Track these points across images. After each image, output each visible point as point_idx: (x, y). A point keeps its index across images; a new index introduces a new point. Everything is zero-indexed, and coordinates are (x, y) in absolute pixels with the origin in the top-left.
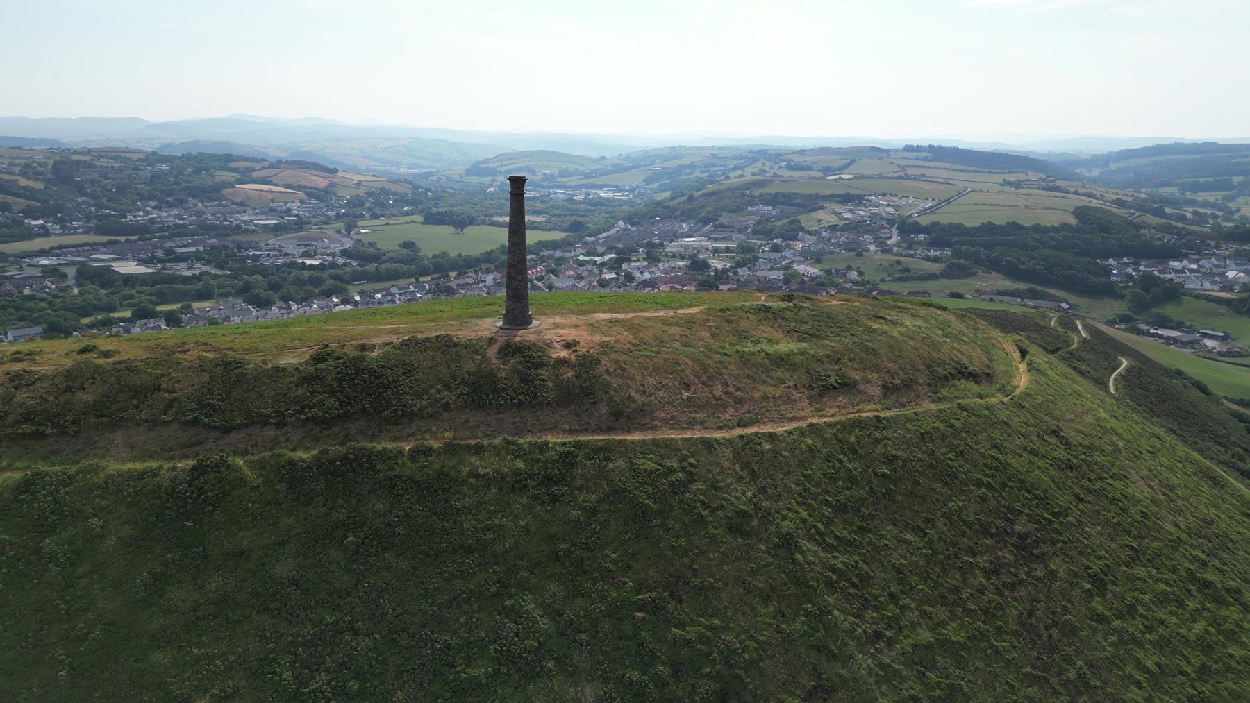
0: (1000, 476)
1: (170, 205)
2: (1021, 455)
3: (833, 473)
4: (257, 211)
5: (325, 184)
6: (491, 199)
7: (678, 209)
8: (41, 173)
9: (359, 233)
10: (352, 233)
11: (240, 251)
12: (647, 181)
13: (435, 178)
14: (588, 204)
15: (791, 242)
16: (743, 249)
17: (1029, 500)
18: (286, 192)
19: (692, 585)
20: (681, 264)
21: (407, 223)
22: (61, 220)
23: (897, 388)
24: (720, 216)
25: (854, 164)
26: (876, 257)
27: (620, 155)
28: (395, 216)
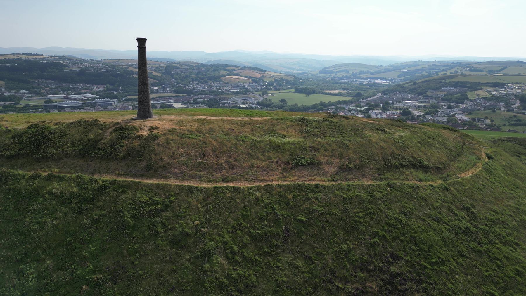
0: (396, 232)
1: (202, 83)
2: (424, 220)
3: (264, 216)
4: (232, 86)
5: (260, 76)
6: (326, 83)
7: (408, 88)
8: (161, 70)
9: (267, 96)
10: (265, 95)
11: (220, 101)
12: (399, 76)
13: (306, 75)
14: (368, 86)
15: (459, 105)
16: (432, 107)
17: (414, 251)
19: (127, 274)
20: (399, 112)
21: (288, 92)
22: (164, 87)
23: (350, 169)
24: (427, 91)
25: (506, 69)
26: (503, 113)
27: (390, 65)
28: (284, 89)
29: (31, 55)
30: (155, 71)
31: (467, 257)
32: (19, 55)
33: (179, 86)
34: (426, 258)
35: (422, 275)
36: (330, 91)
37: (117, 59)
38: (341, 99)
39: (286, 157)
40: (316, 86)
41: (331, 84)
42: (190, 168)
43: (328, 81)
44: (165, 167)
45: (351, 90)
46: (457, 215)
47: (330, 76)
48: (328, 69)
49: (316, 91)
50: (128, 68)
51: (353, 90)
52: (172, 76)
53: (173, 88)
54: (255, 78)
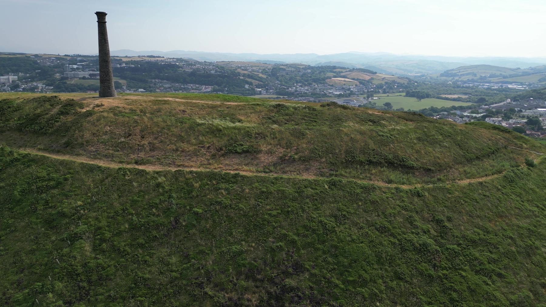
1: (305, 85)
6: (445, 87)
8: (267, 72)
10: (370, 99)
12: (540, 81)
13: (424, 78)
17: (328, 263)
18: (351, 81)
21: (398, 96)
23: (294, 160)
28: (394, 93)
29: (154, 57)
30: (262, 73)
31: (407, 282)
32: (143, 57)
33: (282, 88)
34: (342, 274)
35: (326, 295)
36: (447, 96)
37: (229, 61)
38: (457, 104)
39: (223, 142)
40: (433, 89)
41: (451, 88)
42: (107, 147)
43: (448, 85)
44: (83, 144)
45: (474, 95)
46: (416, 227)
47: (452, 79)
48: (451, 72)
49: (430, 96)
50: (236, 69)
51: (477, 95)
52: (277, 78)
53: (276, 90)
54: (363, 80)
